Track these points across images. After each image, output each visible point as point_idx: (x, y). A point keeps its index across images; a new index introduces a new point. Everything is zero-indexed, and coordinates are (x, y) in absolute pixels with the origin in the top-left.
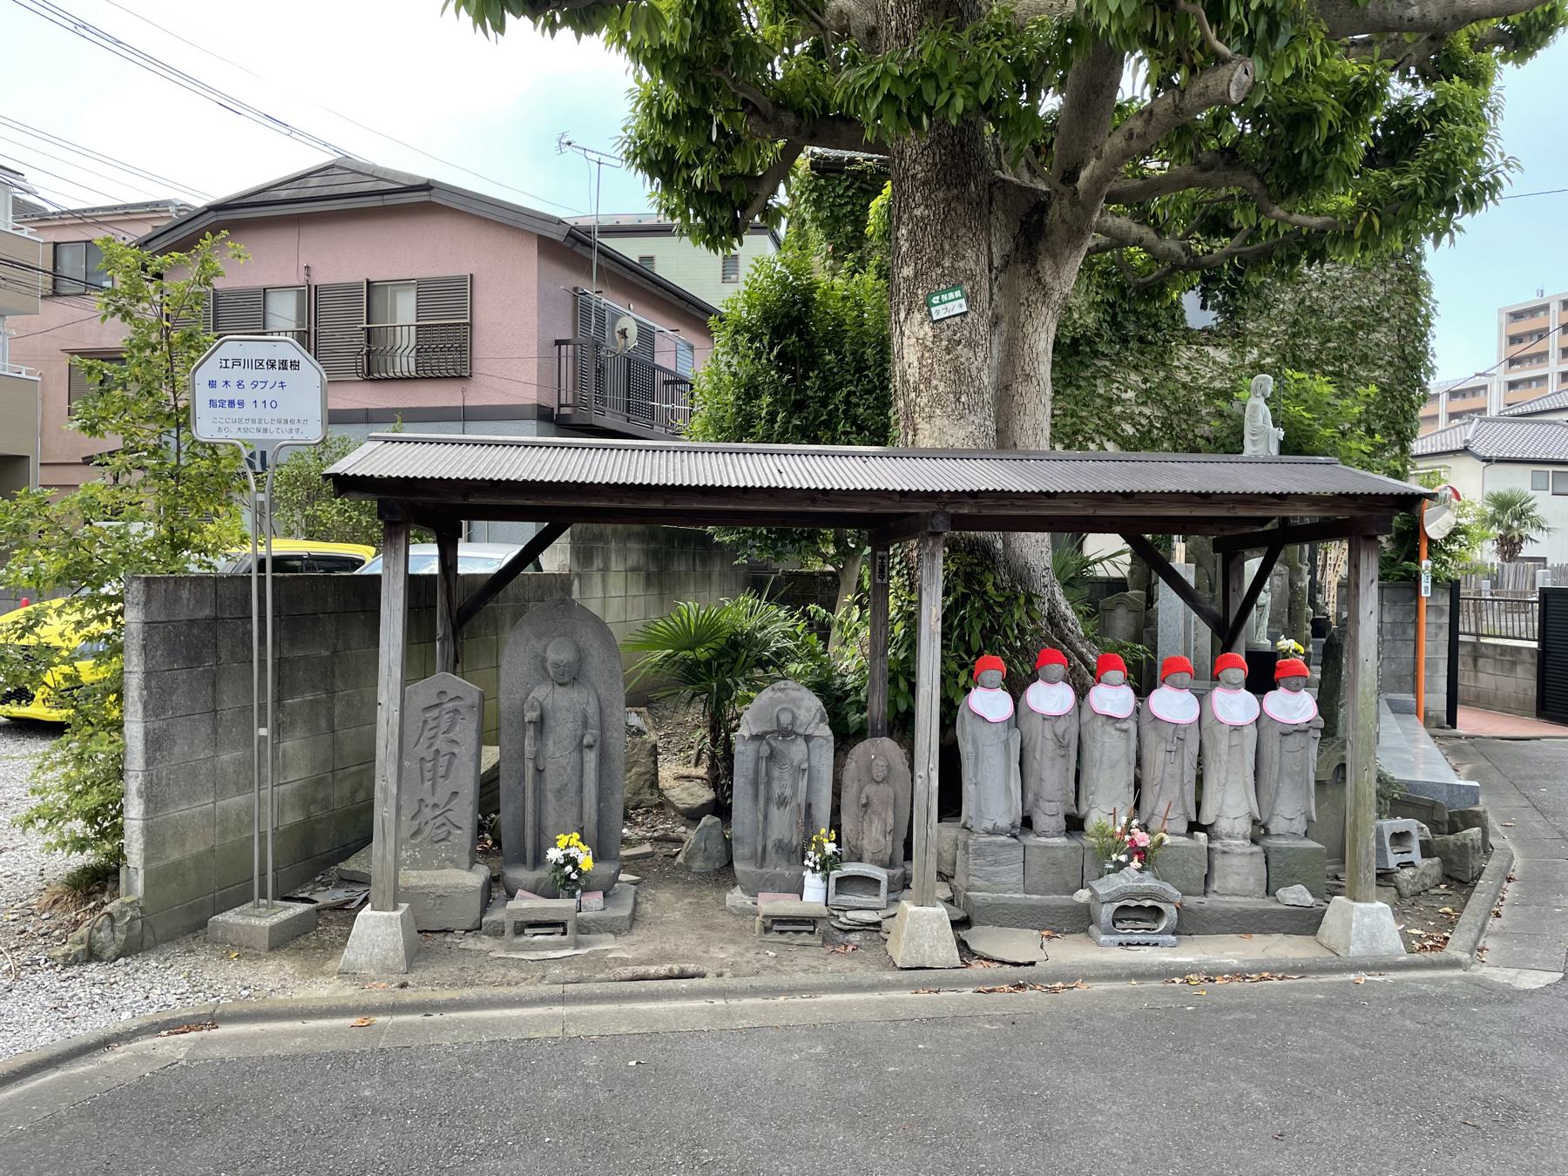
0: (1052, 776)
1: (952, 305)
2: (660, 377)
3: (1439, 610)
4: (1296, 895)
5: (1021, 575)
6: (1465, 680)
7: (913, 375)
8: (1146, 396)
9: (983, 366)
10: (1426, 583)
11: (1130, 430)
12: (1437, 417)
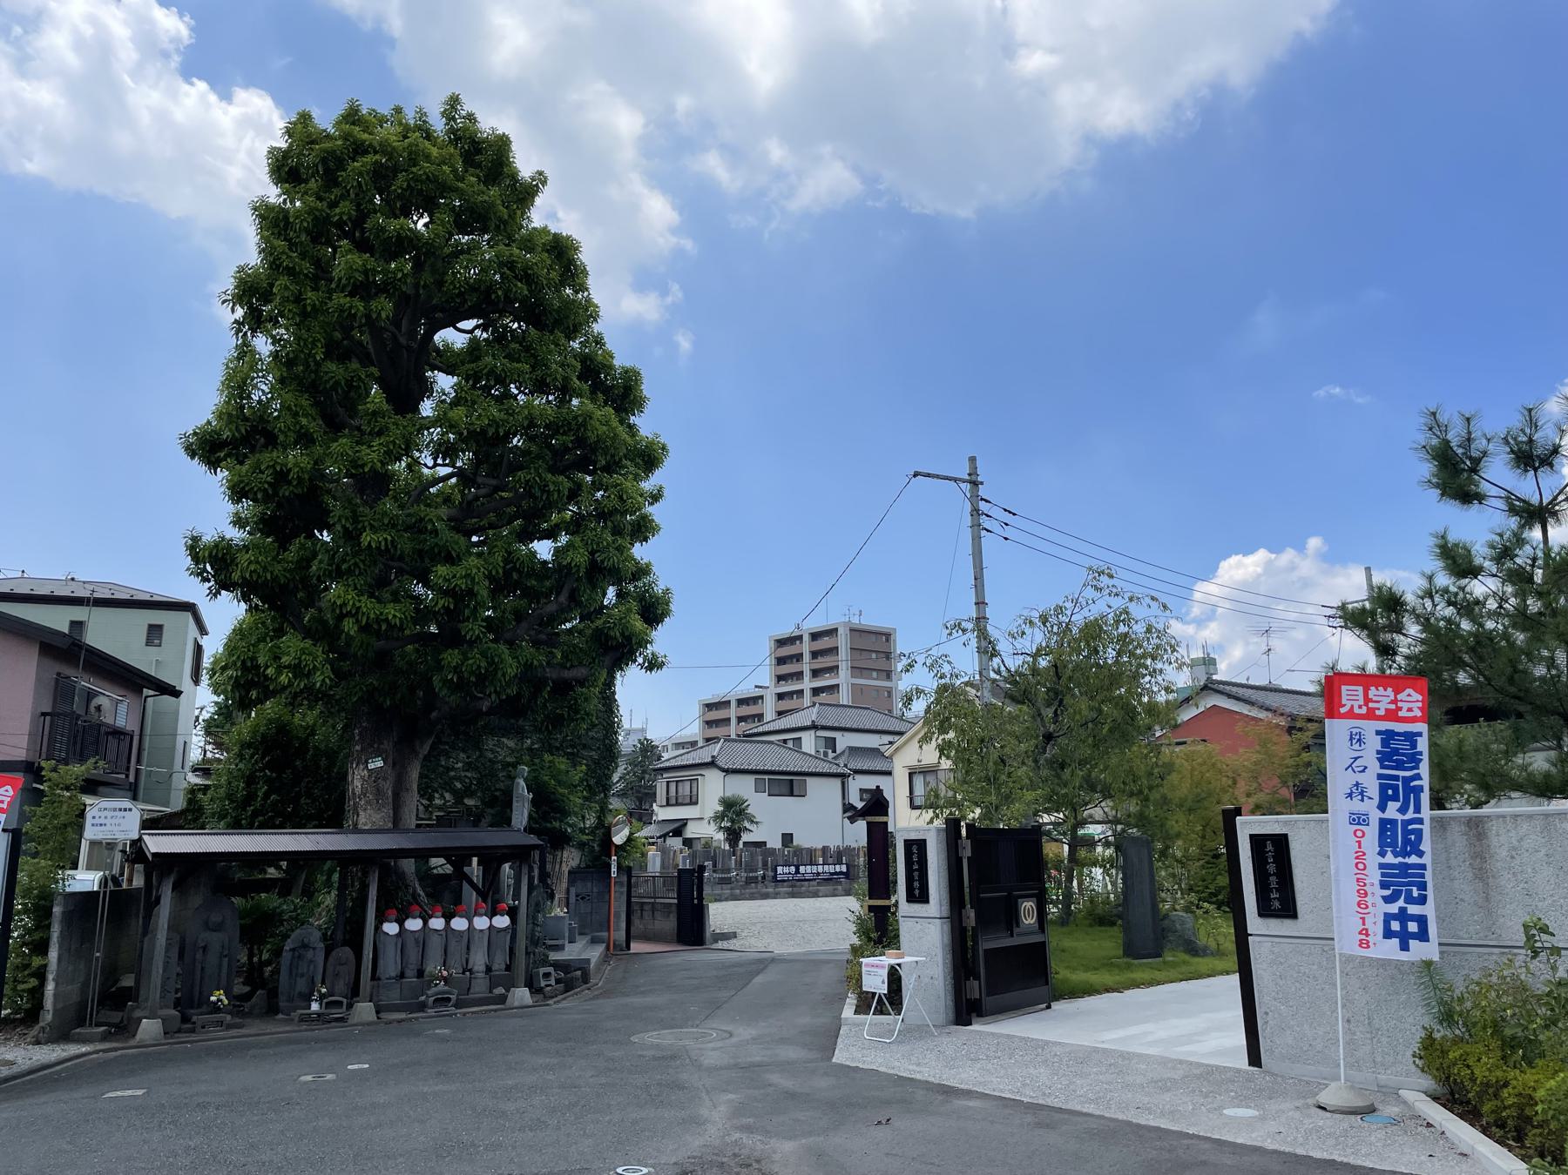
0: (413, 955)
1: (378, 763)
2: (103, 729)
3: (621, 884)
4: (500, 990)
5: (401, 876)
6: (637, 925)
7: (358, 791)
8: (469, 766)
9: (388, 787)
10: (614, 869)
11: (459, 785)
12: (729, 720)
